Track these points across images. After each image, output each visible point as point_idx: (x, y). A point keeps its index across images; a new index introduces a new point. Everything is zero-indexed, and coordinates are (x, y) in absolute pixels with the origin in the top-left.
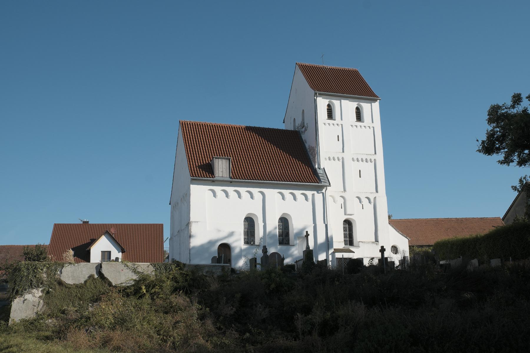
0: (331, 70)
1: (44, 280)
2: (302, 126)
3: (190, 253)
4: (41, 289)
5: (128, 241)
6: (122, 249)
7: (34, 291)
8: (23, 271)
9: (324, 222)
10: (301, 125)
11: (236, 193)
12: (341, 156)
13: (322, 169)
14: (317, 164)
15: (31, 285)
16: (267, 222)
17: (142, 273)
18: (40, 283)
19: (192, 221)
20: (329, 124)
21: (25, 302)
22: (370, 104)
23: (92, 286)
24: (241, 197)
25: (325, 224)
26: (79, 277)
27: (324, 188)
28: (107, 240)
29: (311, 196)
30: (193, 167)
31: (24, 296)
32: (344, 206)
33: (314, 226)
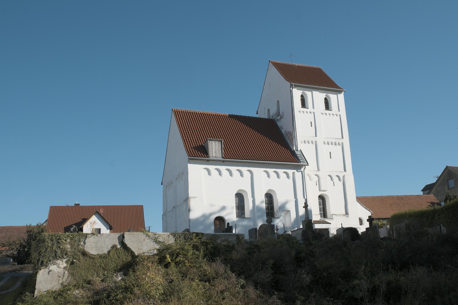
0: (299, 67)
1: (68, 251)
2: (277, 115)
4: (65, 260)
5: (114, 220)
6: (110, 227)
7: (59, 262)
8: (47, 242)
9: (304, 197)
10: (276, 114)
11: (227, 172)
12: (314, 139)
15: (56, 256)
16: (256, 197)
18: (64, 254)
20: (303, 112)
21: (50, 273)
23: (116, 256)
24: (233, 175)
25: (304, 199)
26: (103, 248)
28: (97, 219)
29: (292, 174)
31: (49, 267)
32: (319, 183)
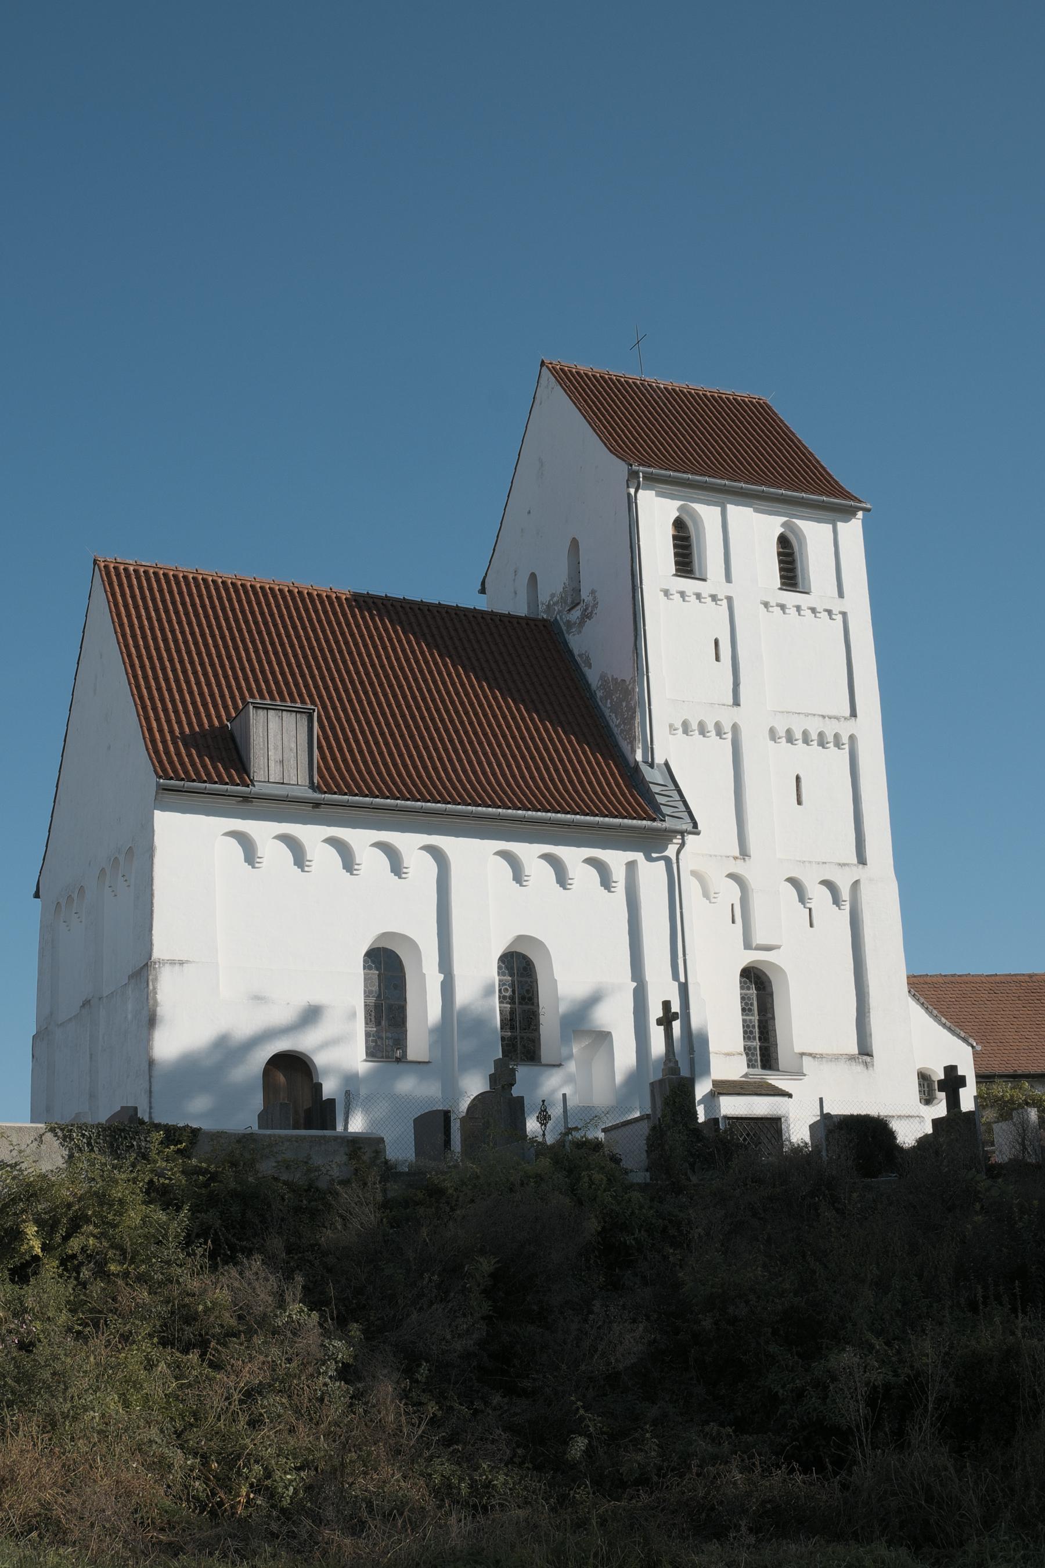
0: (672, 394)
2: (569, 601)
3: (150, 1092)
9: (675, 976)
10: (563, 600)
12: (728, 717)
13: (659, 765)
14: (640, 746)
17: (13, 1166)
19: (162, 957)
20: (682, 594)
22: (830, 526)
27: (670, 841)
30: (164, 742)
33: (636, 990)
